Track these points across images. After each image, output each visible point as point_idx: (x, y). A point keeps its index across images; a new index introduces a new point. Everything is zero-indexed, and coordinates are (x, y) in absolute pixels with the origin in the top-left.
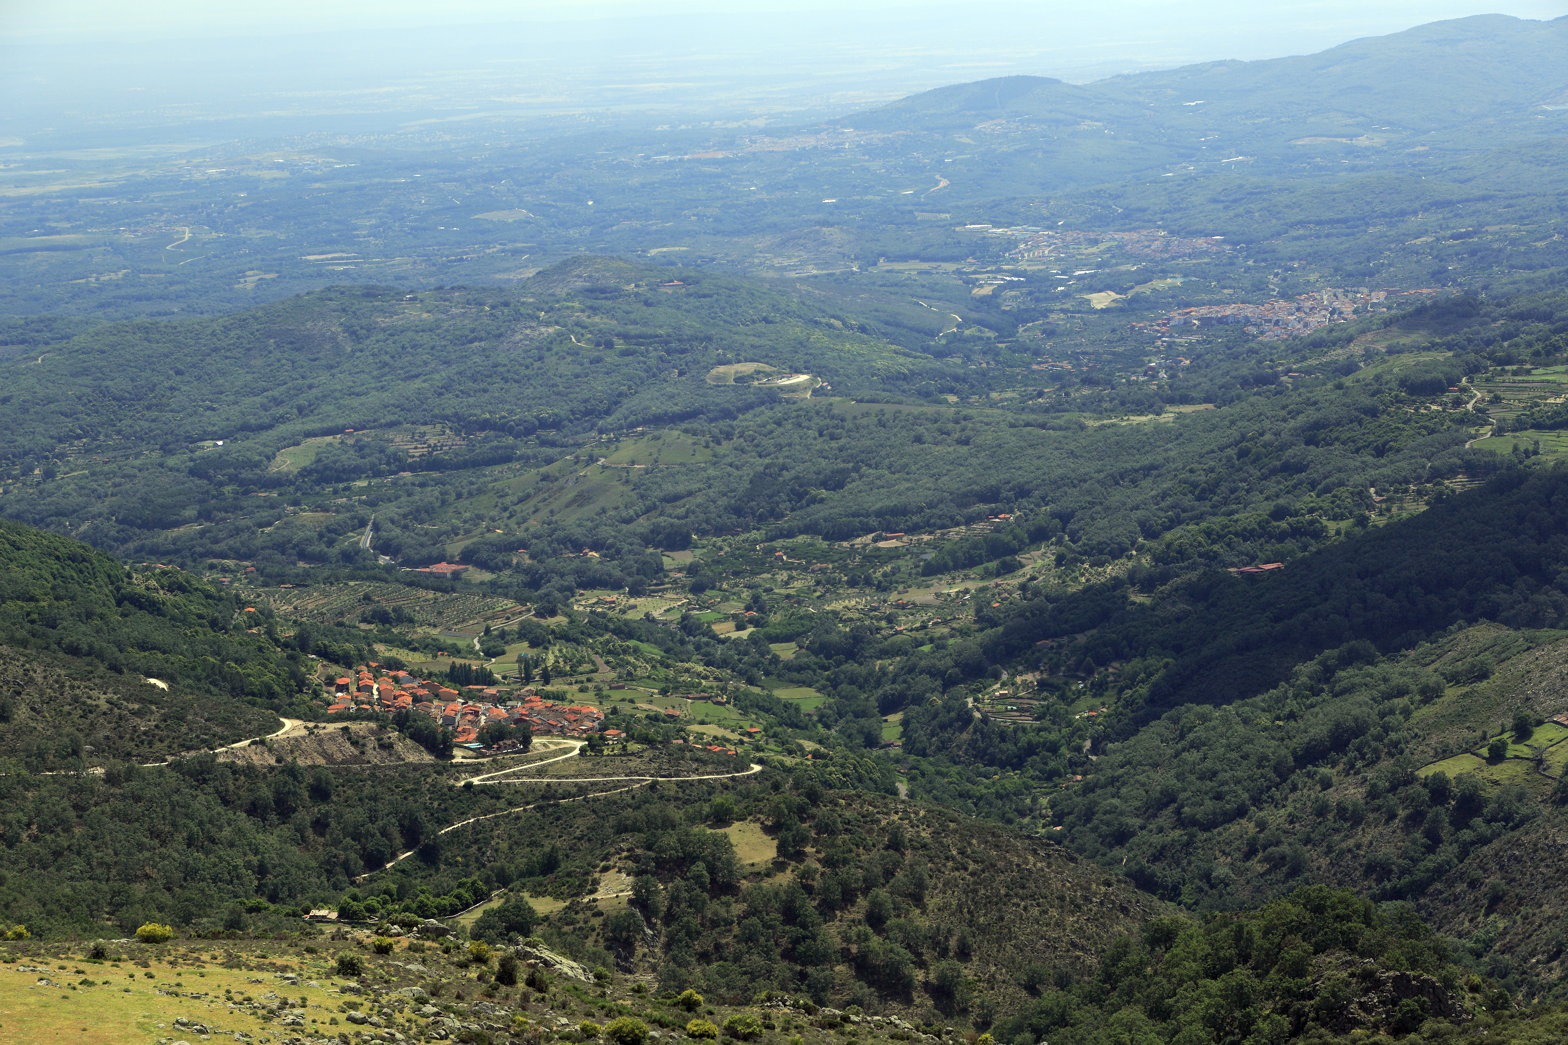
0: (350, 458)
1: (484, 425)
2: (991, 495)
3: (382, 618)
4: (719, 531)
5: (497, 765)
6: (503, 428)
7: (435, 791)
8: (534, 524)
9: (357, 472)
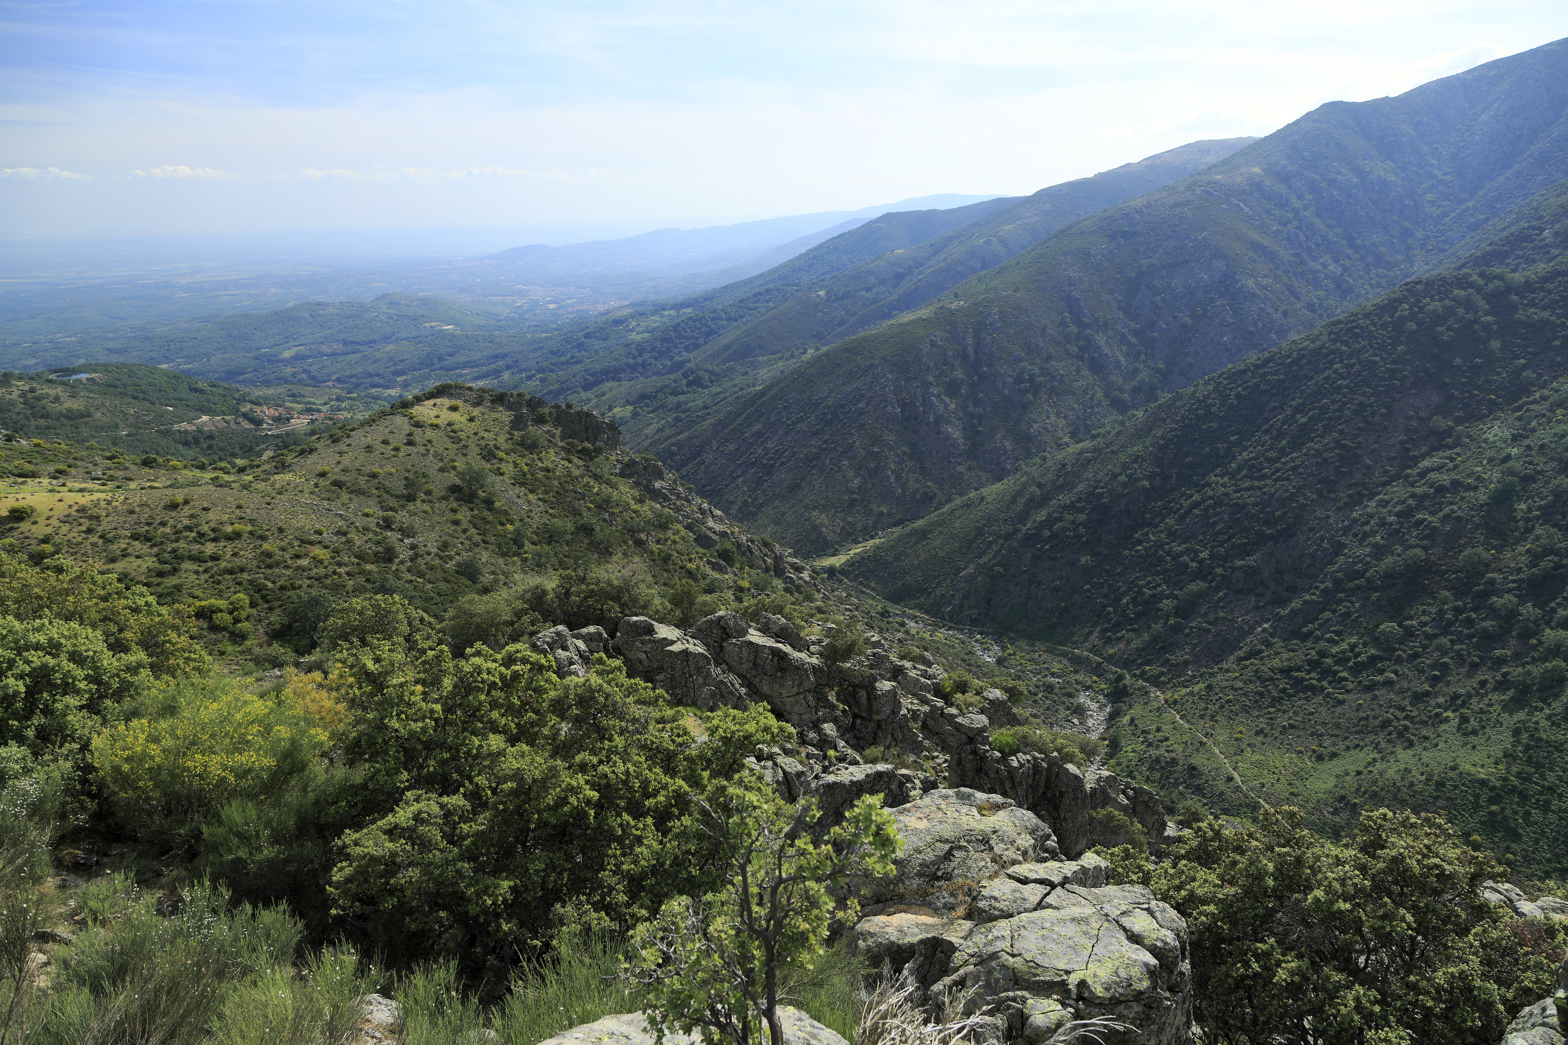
0: (307, 353)
1: (352, 342)
2: (496, 357)
3: (293, 395)
4: (415, 369)
5: (277, 428)
6: (358, 343)
7: (255, 437)
8: (359, 370)
9: (309, 357)
